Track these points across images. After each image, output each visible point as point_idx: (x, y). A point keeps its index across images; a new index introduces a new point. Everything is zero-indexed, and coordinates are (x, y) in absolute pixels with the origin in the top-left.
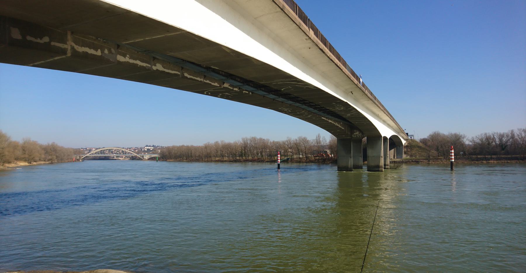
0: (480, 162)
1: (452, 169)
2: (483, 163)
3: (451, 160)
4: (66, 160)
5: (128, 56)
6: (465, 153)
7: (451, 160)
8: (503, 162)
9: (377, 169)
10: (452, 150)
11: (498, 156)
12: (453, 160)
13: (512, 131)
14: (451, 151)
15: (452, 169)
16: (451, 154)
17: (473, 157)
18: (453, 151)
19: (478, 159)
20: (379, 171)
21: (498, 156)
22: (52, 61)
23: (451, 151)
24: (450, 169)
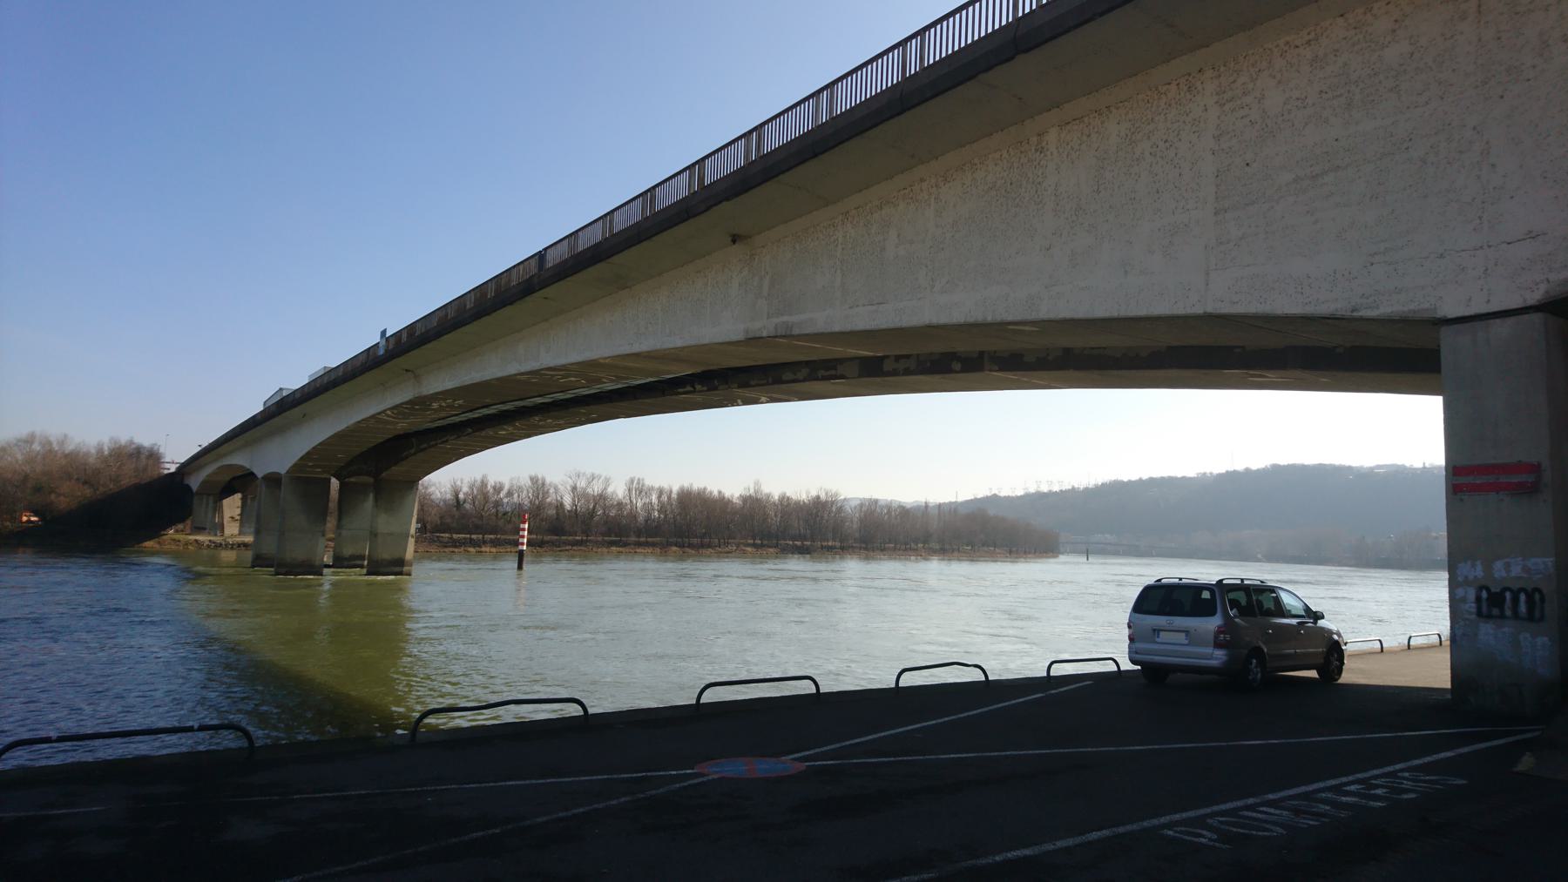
0: (462, 549)
1: (520, 567)
2: (468, 552)
3: (520, 547)
4: (87, 707)
5: (1250, 677)
6: (426, 527)
7: (520, 547)
8: (509, 550)
9: (397, 569)
10: (524, 523)
11: (499, 536)
12: (525, 548)
13: (484, 477)
14: (522, 526)
15: (520, 567)
16: (521, 533)
17: (442, 537)
18: (526, 526)
19: (456, 544)
20: (401, 573)
21: (499, 536)
22: (954, 719)
23: (522, 526)
24: (516, 565)
